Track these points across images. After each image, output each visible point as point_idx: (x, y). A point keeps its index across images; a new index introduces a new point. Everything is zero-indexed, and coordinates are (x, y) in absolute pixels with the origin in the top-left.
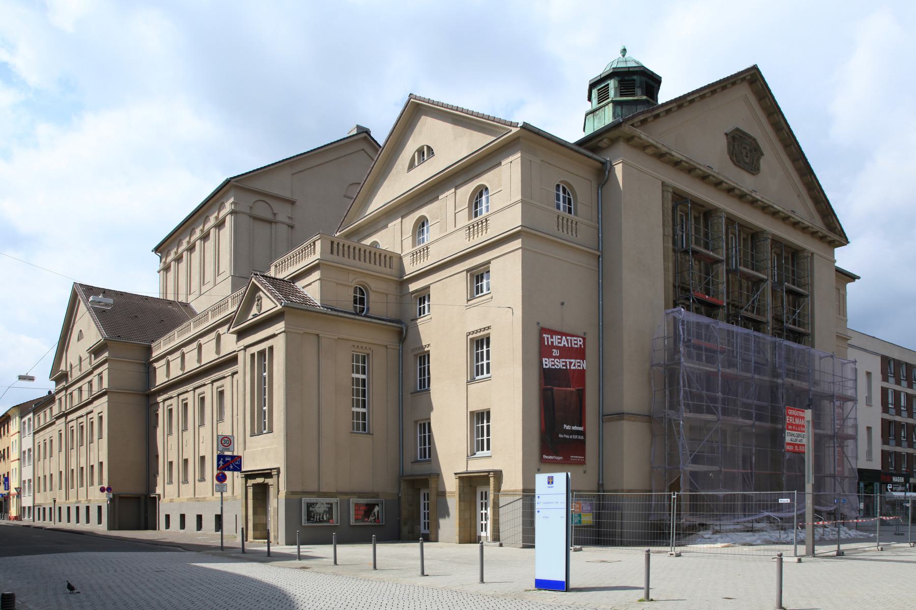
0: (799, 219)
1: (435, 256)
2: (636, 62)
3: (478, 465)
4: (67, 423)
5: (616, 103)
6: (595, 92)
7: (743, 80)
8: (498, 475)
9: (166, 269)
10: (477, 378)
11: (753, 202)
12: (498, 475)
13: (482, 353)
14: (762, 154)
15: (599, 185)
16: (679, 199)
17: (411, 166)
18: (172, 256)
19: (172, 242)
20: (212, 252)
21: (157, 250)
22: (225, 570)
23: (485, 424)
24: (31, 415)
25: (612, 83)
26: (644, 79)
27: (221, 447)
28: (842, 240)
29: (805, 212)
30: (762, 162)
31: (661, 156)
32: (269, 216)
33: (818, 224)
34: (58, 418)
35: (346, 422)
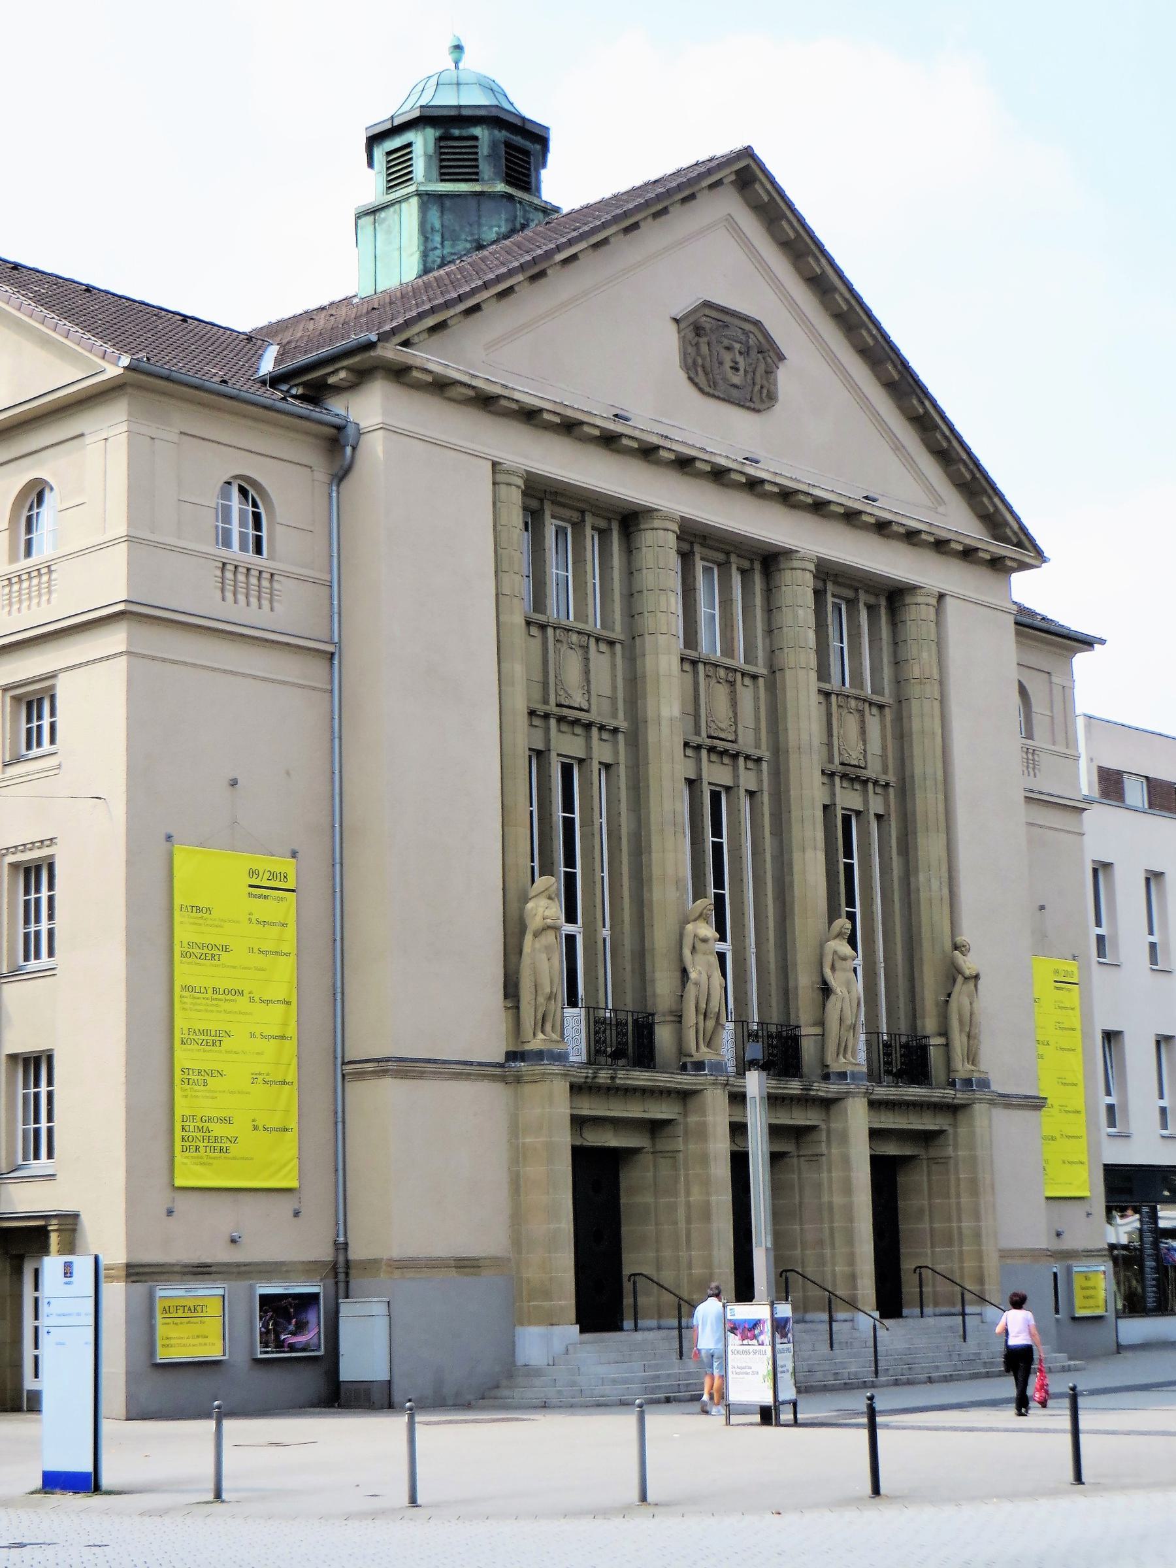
0: (888, 516)
2: (491, 88)
6: (379, 153)
8: (70, 1222)
10: (33, 964)
12: (70, 1222)
13: (38, 900)
14: (781, 357)
15: (334, 476)
16: (541, 498)
22: (121, 1315)
23: (43, 1089)
25: (421, 142)
26: (502, 135)
29: (912, 491)
30: (785, 379)
31: (485, 402)
33: (958, 521)
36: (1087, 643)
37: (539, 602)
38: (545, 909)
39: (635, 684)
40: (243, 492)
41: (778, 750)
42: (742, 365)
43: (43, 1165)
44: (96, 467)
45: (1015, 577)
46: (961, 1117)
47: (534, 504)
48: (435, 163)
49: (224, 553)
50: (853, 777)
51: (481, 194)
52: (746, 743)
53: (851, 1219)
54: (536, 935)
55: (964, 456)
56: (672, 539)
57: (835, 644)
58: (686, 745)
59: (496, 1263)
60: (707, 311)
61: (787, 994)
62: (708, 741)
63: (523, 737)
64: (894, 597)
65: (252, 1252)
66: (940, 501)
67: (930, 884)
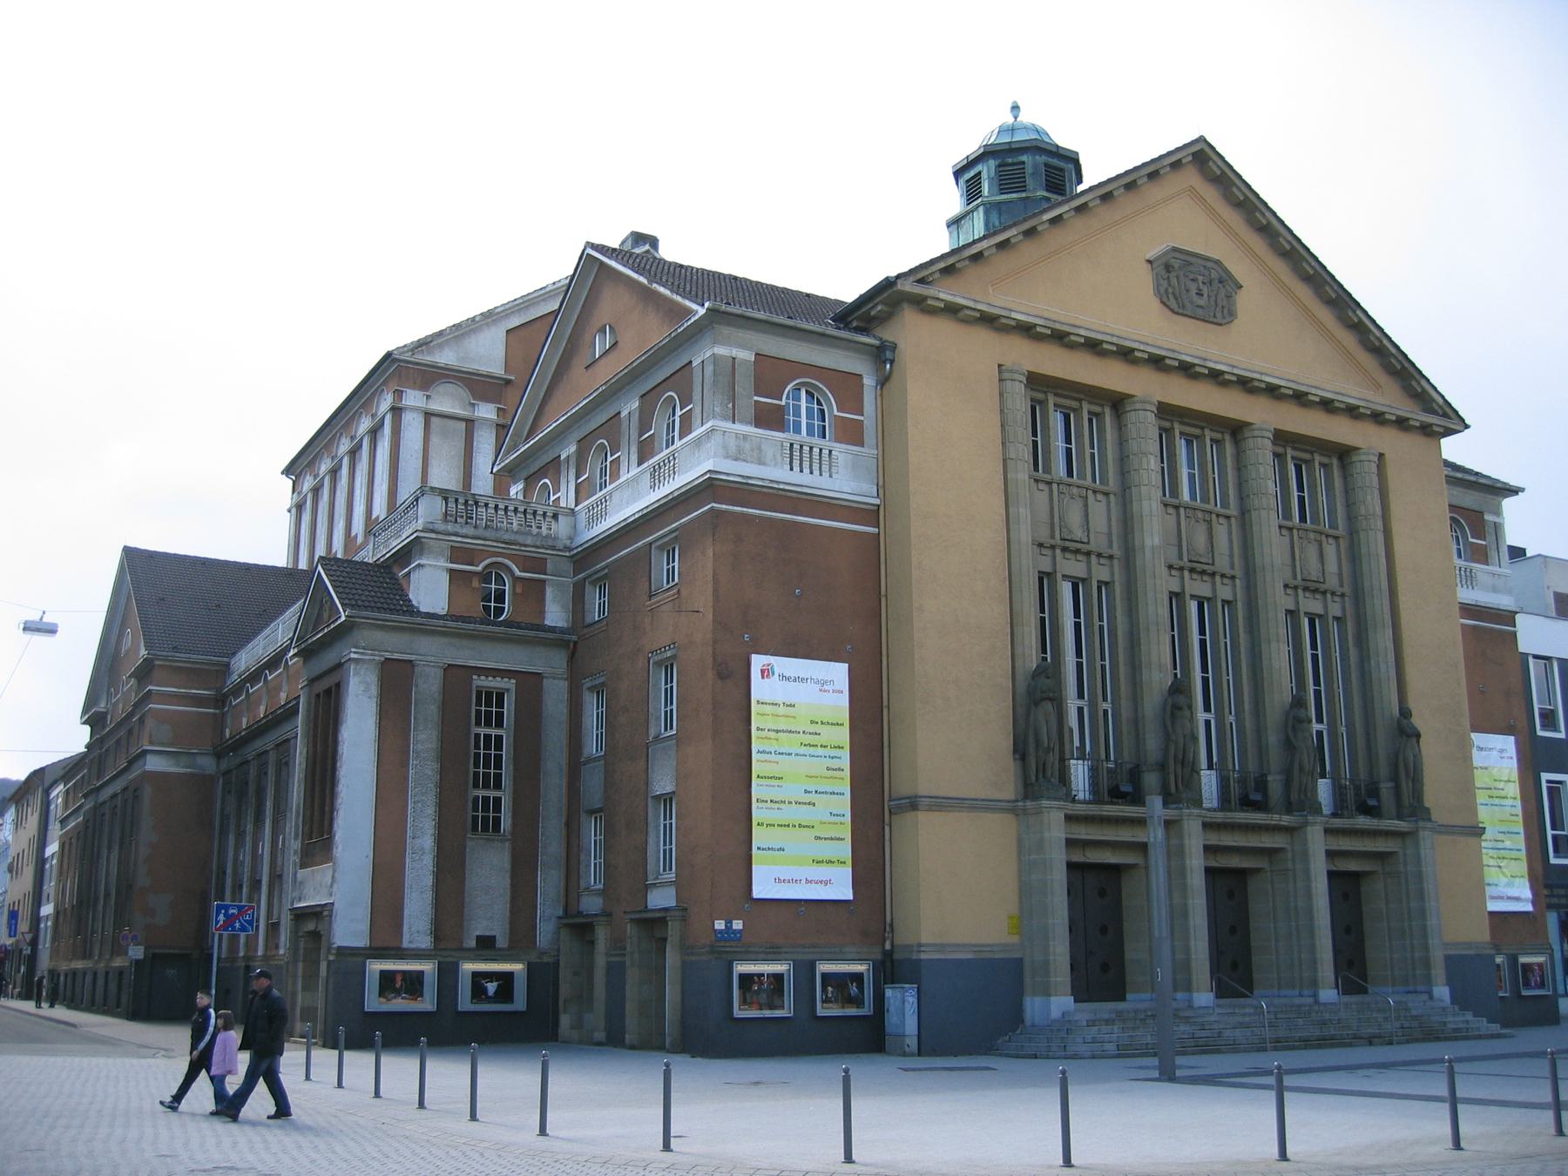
6: (961, 181)
7: (1176, 165)
16: (1036, 381)
21: (288, 471)
25: (987, 170)
28: (1452, 422)
30: (1243, 301)
31: (989, 321)
33: (1390, 399)
36: (1514, 491)
39: (1128, 524)
41: (1250, 572)
42: (1205, 291)
47: (1280, 450)
48: (996, 182)
52: (1098, 543)
53: (1311, 918)
55: (1393, 351)
58: (1286, 586)
60: (1177, 255)
63: (1030, 564)
64: (1344, 454)
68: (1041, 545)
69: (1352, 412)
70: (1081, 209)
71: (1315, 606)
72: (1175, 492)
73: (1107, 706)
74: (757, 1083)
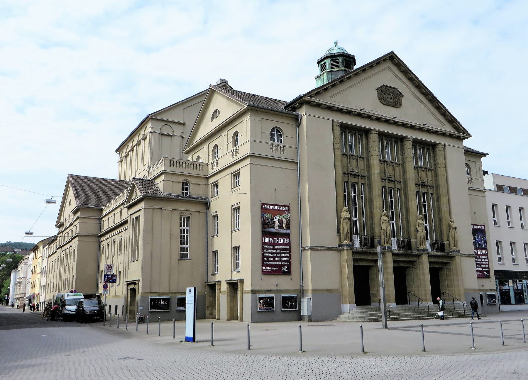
1: (220, 167)
3: (236, 277)
4: (62, 252)
5: (328, 72)
6: (320, 65)
8: (242, 281)
9: (121, 161)
11: (396, 123)
12: (242, 281)
16: (345, 128)
17: (212, 119)
18: (124, 154)
19: (124, 146)
20: (141, 154)
24: (48, 246)
25: (327, 61)
27: (106, 270)
28: (466, 135)
29: (436, 122)
30: (403, 100)
31: (330, 108)
32: (171, 133)
33: (448, 128)
34: (58, 249)
35: (176, 252)
36: (485, 155)
37: (417, 163)
38: (345, 214)
39: (369, 167)
40: (277, 130)
41: (405, 180)
42: (393, 97)
43: (237, 270)
44: (245, 126)
45: (464, 141)
46: (453, 259)
47: (415, 144)
49: (272, 142)
50: (425, 185)
51: (339, 70)
52: (430, 183)
54: (344, 220)
56: (411, 143)
57: (358, 145)
58: (416, 184)
59: (337, 290)
61: (409, 232)
62: (388, 178)
64: (434, 146)
65: (281, 287)
66: (444, 125)
67: (444, 208)
68: (344, 173)
69: (436, 133)
70: (356, 74)
71: (425, 190)
72: (417, 163)
73: (364, 219)
74: (267, 330)
